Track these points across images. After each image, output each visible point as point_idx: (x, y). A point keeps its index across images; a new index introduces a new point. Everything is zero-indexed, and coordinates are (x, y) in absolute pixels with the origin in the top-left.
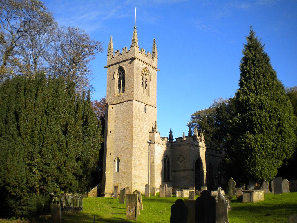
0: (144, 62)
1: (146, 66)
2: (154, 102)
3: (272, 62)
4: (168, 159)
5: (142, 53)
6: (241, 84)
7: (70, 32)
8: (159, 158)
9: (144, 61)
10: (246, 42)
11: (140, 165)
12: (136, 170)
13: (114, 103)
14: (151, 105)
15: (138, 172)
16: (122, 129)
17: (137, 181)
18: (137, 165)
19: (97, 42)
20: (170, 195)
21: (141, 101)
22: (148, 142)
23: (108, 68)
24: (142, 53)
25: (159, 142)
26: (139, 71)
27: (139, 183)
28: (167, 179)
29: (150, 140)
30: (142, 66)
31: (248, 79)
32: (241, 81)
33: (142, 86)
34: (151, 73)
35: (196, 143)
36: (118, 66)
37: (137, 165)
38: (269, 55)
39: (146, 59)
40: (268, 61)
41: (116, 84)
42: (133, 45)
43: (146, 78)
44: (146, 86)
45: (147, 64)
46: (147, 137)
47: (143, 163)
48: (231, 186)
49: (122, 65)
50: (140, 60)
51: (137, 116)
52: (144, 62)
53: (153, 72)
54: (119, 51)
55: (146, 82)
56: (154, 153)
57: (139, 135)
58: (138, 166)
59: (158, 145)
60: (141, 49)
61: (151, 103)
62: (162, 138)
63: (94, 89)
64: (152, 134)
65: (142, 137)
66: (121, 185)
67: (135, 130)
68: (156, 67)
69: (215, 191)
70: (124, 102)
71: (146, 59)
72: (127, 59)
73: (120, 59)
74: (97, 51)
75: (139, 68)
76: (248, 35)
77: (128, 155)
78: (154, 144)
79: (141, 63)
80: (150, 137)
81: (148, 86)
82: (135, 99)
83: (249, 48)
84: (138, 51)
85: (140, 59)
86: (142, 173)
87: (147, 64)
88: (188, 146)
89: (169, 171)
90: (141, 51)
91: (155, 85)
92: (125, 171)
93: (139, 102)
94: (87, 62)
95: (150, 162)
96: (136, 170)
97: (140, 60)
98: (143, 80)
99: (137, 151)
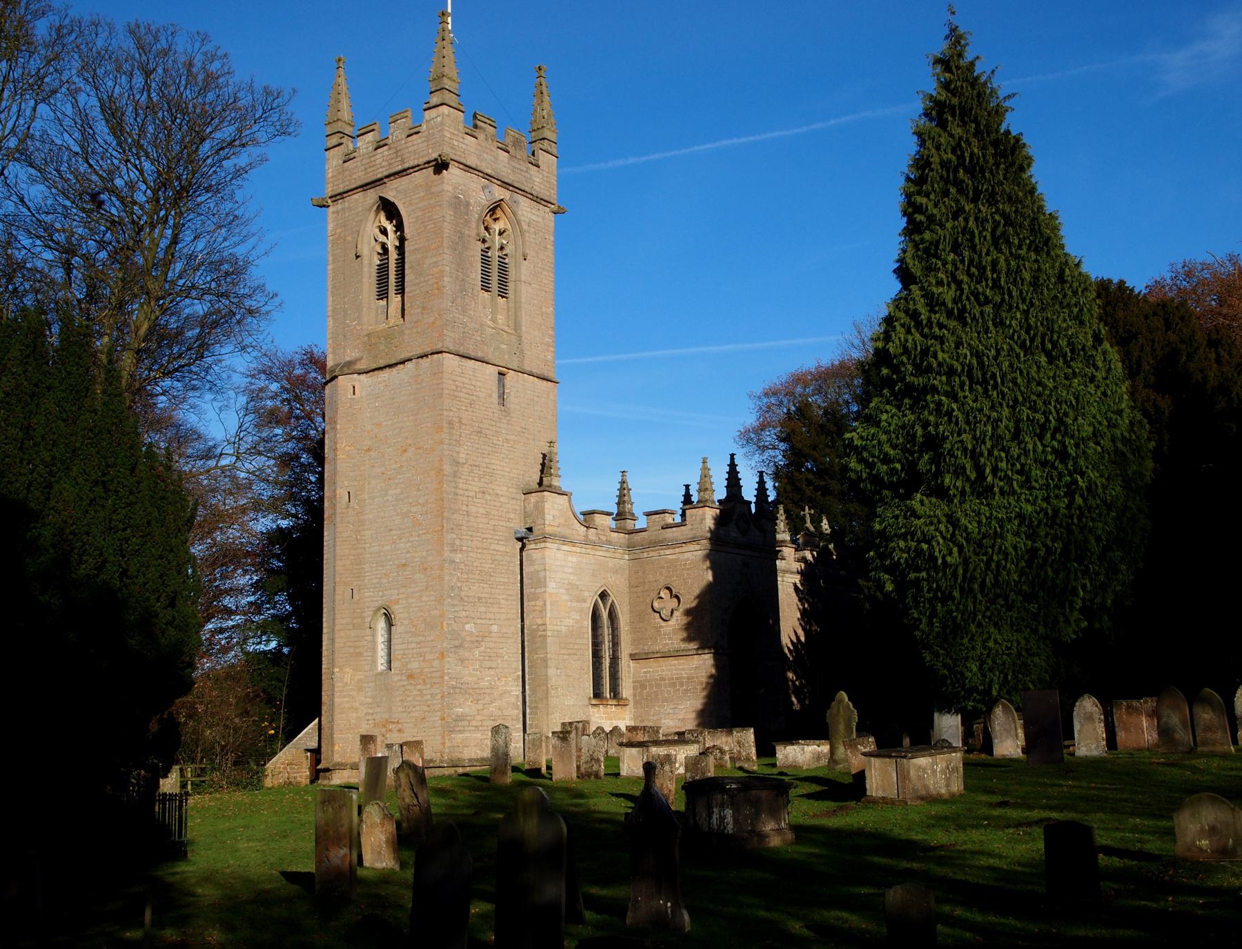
0: (488, 177)
1: (499, 193)
2: (539, 353)
3: (1042, 175)
4: (612, 605)
5: (481, 136)
6: (904, 274)
7: (140, 47)
8: (569, 604)
9: (489, 171)
10: (929, 82)
11: (484, 637)
12: (462, 661)
13: (361, 366)
14: (528, 369)
15: (471, 668)
16: (397, 484)
17: (467, 710)
18: (468, 639)
19: (267, 91)
20: (595, 768)
21: (480, 355)
22: (519, 535)
23: (331, 209)
24: (481, 136)
25: (566, 531)
26: (467, 222)
27: (479, 718)
28: (608, 696)
29: (528, 526)
30: (479, 194)
31: (929, 253)
32: (901, 261)
33: (486, 288)
34: (525, 227)
35: (733, 534)
36: (372, 196)
37: (468, 639)
38: (1033, 146)
39: (502, 164)
40: (1022, 169)
41: (366, 275)
42: (435, 100)
43: (502, 248)
44: (503, 283)
45: (506, 185)
46: (512, 516)
47: (495, 628)
48: (841, 727)
49: (391, 192)
50: (468, 168)
51: (463, 421)
52: (488, 177)
53: (535, 218)
54: (409, 114)
55: (503, 269)
56: (542, 583)
57: (473, 509)
58: (472, 642)
59: (566, 548)
60: (475, 117)
61: (527, 362)
62: (582, 517)
63: (277, 301)
64: (533, 498)
65: (488, 514)
66: (400, 731)
67: (456, 487)
68: (552, 194)
69: (793, 744)
70: (403, 362)
71: (502, 164)
72: (411, 164)
73: (383, 163)
74: (271, 129)
75: (468, 204)
76: (940, 47)
77: (424, 599)
78: (542, 545)
79: (476, 182)
80: (526, 515)
81: (511, 286)
82: (452, 348)
83: (938, 111)
84: (461, 127)
85: (468, 164)
86: (492, 672)
87: (506, 185)
88: (698, 547)
89: (615, 660)
90: (476, 126)
91: (548, 279)
92: (414, 665)
93: (470, 358)
94: (239, 173)
95: (527, 622)
96: (462, 661)
97: (468, 168)
98: (486, 261)
99: (465, 576)
